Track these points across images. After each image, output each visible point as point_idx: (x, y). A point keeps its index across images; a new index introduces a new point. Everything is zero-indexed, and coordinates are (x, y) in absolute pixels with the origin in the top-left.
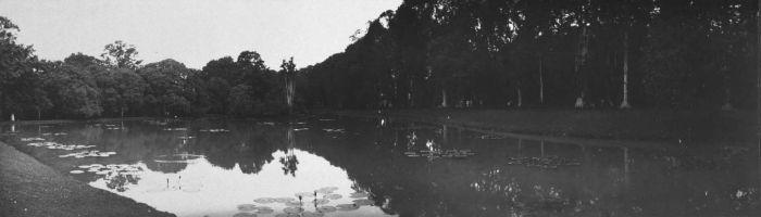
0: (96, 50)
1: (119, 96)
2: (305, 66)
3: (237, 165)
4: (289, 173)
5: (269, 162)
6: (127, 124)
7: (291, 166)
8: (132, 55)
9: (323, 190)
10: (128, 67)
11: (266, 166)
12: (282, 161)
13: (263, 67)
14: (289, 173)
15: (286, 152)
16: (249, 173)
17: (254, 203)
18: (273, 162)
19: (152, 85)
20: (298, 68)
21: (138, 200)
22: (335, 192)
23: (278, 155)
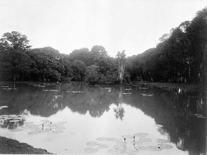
0: (81, 48)
1: (13, 67)
2: (131, 55)
3: (88, 112)
4: (119, 118)
5: (107, 111)
6: (17, 85)
7: (120, 114)
8: (24, 42)
9: (139, 134)
10: (21, 49)
11: (105, 113)
12: (115, 110)
13: (106, 55)
14: (119, 118)
15: (118, 105)
16: (95, 116)
17: (97, 141)
18: (109, 111)
19: (37, 62)
20: (126, 57)
21: (21, 141)
22: (147, 137)
23: (113, 106)
